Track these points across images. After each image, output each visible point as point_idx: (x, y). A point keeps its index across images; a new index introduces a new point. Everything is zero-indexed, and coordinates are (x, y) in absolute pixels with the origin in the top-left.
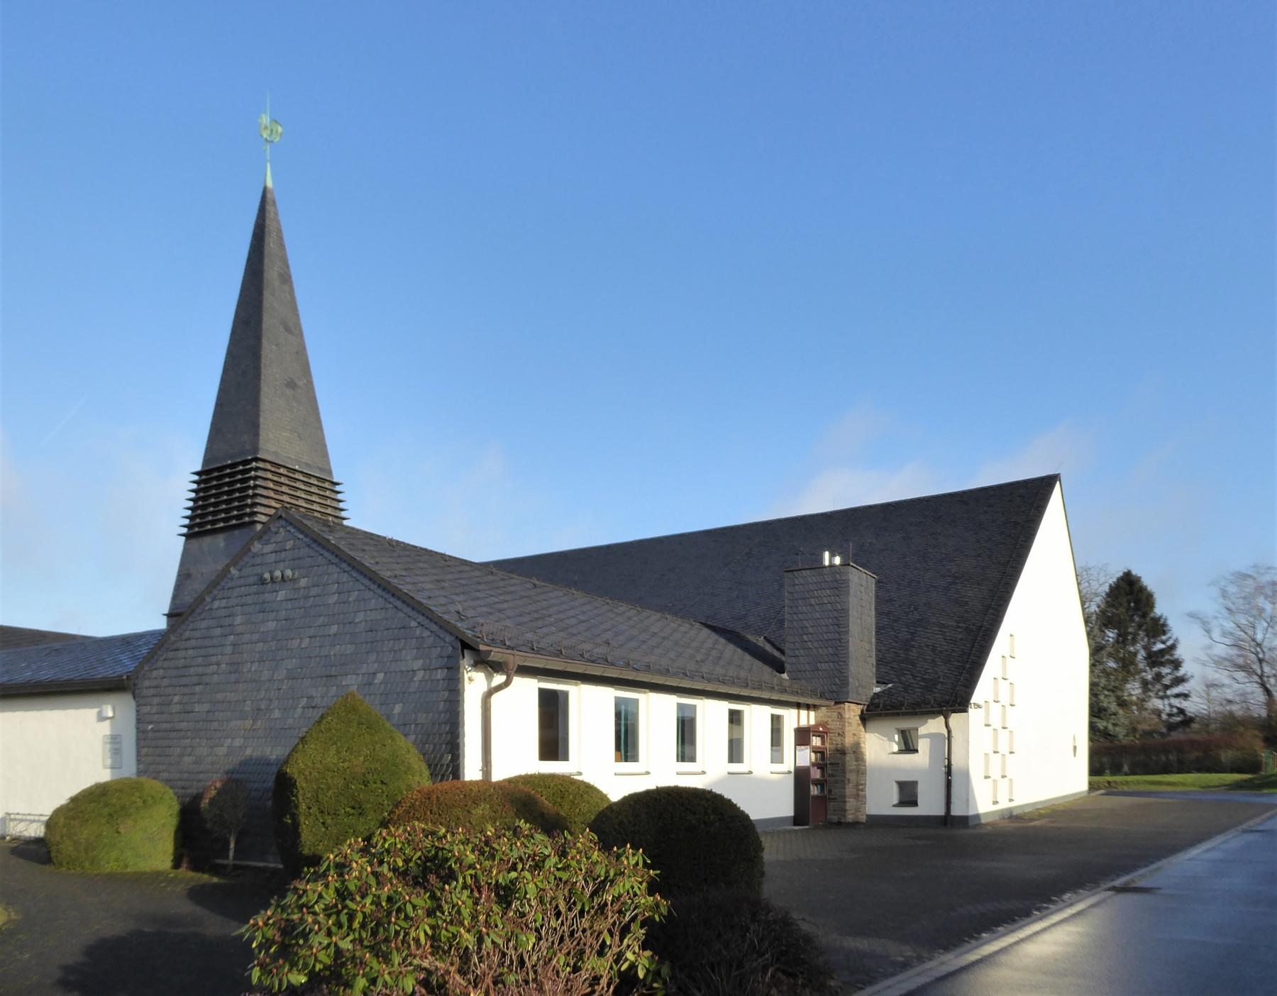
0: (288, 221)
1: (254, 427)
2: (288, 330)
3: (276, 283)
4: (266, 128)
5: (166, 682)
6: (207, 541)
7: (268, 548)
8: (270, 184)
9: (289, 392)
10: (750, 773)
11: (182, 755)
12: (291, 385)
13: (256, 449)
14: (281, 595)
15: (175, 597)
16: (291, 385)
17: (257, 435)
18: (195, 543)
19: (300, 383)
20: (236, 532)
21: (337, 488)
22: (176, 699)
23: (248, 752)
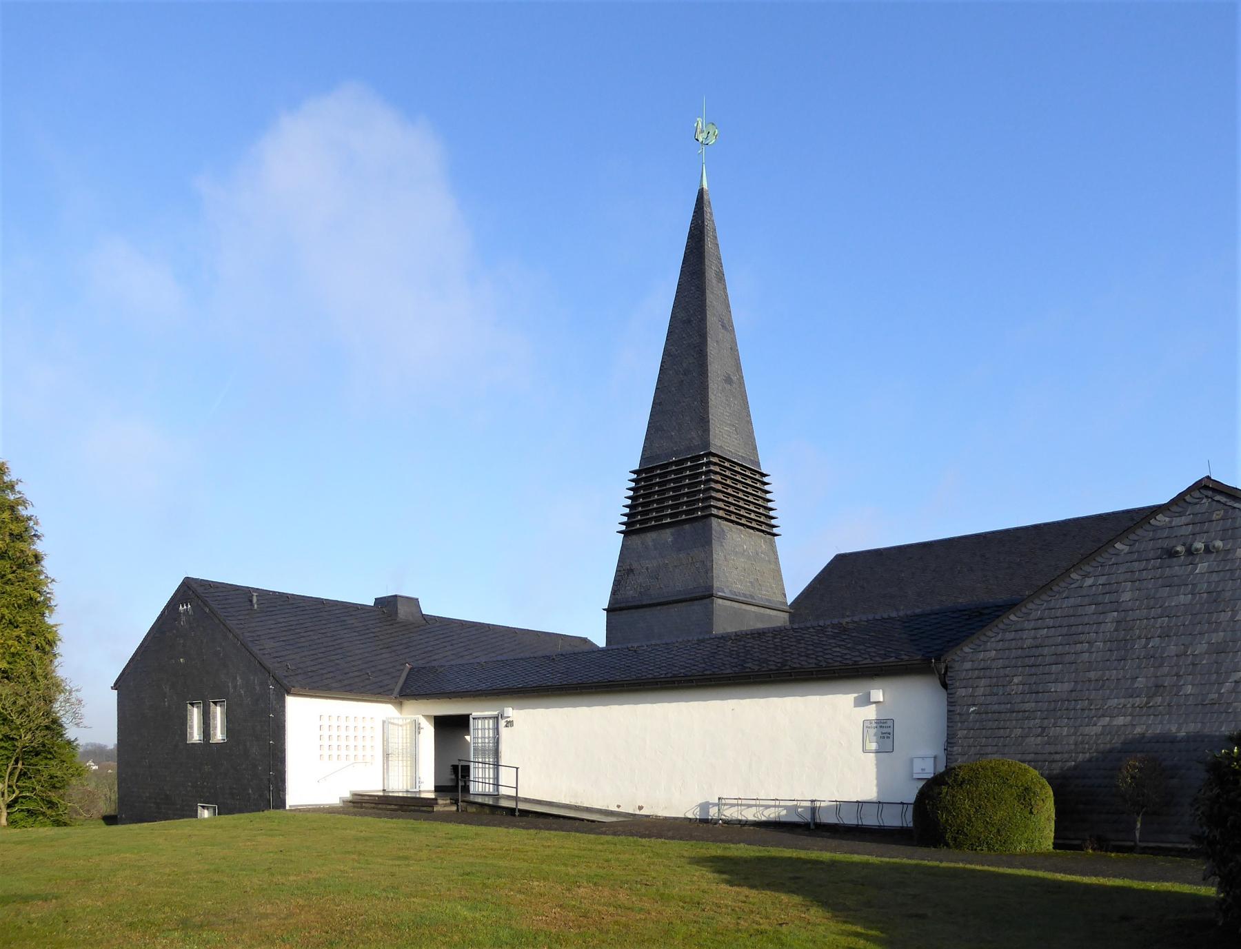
0: (718, 216)
1: (703, 422)
2: (723, 326)
3: (714, 281)
4: (702, 131)
5: (1000, 663)
6: (650, 537)
7: (1184, 520)
8: (705, 186)
9: (728, 387)
10: (935, 757)
11: (1023, 737)
12: (728, 380)
13: (707, 444)
14: (1202, 567)
15: (614, 592)
16: (728, 380)
17: (706, 430)
18: (636, 540)
19: (735, 378)
20: (687, 527)
21: (765, 479)
22: (1016, 680)
23: (1138, 730)
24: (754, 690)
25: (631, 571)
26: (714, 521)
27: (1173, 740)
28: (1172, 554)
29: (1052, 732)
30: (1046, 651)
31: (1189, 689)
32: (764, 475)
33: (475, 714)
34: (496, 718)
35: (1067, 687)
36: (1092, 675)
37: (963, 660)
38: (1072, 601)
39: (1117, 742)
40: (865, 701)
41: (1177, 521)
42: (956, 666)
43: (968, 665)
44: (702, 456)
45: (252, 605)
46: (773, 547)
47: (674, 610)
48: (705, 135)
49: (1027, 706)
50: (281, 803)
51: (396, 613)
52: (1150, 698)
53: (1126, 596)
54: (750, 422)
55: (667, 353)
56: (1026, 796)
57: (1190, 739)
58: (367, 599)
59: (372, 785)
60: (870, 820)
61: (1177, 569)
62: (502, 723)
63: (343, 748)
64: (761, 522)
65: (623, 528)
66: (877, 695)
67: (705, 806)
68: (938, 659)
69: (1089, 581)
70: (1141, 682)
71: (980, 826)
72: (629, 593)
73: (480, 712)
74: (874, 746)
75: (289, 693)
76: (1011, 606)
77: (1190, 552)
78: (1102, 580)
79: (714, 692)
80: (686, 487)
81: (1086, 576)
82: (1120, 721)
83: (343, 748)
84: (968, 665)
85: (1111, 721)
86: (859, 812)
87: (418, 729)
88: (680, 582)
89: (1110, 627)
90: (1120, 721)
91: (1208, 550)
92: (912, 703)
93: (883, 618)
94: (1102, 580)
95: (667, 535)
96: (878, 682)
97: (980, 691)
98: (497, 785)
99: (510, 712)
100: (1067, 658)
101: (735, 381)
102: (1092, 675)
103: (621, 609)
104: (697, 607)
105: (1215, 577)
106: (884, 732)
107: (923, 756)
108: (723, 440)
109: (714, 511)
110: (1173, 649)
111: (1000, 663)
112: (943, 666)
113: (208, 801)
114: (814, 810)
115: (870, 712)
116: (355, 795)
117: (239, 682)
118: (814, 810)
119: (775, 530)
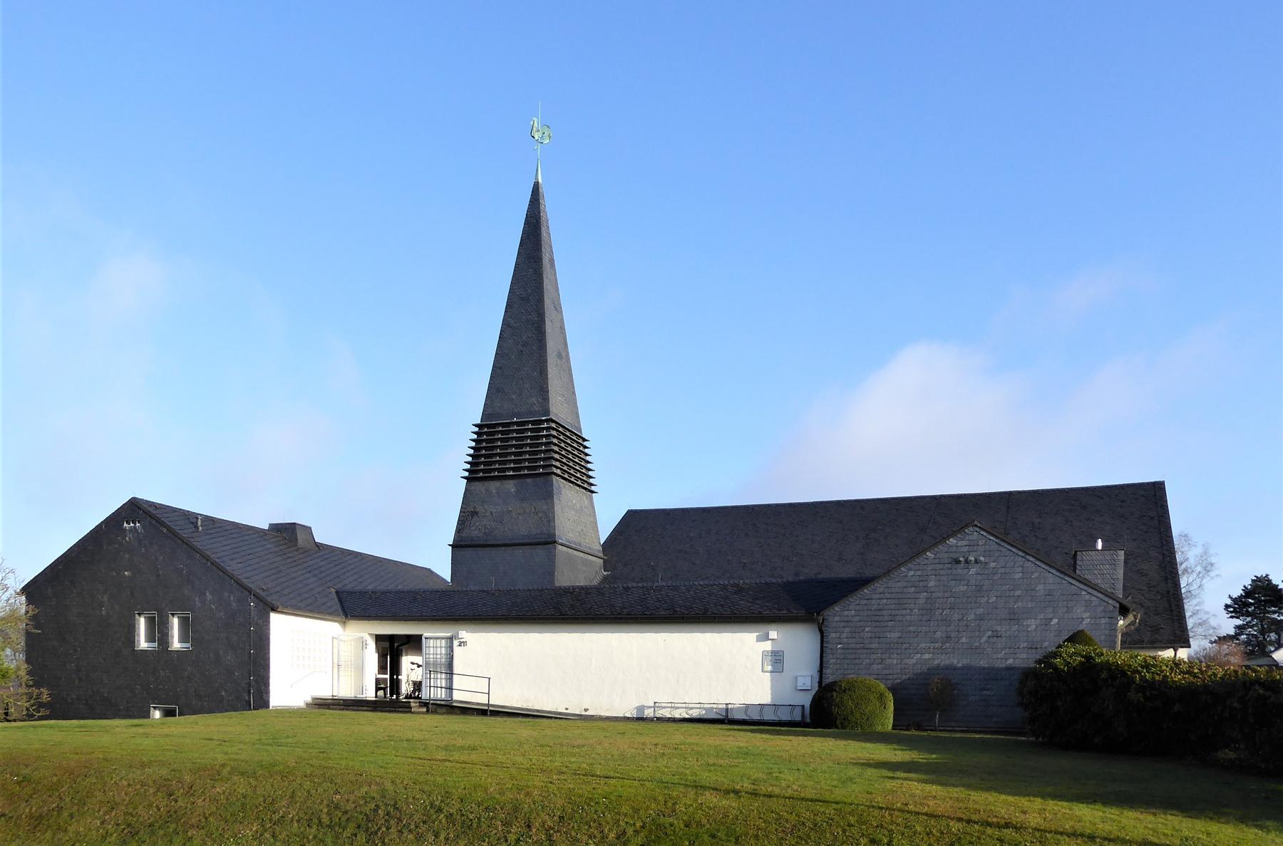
1: (543, 391)
5: (857, 618)
6: (494, 486)
13: (547, 412)
14: (973, 571)
15: (458, 531)
17: (546, 399)
18: (479, 486)
20: (529, 480)
24: (681, 627)
25: (474, 513)
26: (555, 478)
27: (955, 669)
28: (958, 562)
29: (888, 661)
30: (885, 613)
31: (964, 640)
32: (584, 440)
33: (426, 635)
34: (451, 639)
35: (897, 635)
36: (911, 629)
37: (835, 615)
38: (900, 584)
39: (925, 668)
40: (766, 638)
41: (960, 543)
42: (830, 619)
43: (837, 618)
44: (542, 422)
45: (196, 527)
46: (591, 499)
47: (519, 552)
48: (540, 134)
49: (873, 646)
50: (265, 704)
51: (296, 539)
52: (944, 643)
53: (932, 584)
54: (574, 393)
55: (505, 323)
56: (881, 697)
57: (963, 668)
58: (262, 522)
59: (326, 692)
60: (769, 716)
61: (960, 570)
62: (456, 643)
63: (314, 659)
64: (584, 483)
65: (467, 474)
66: (773, 634)
67: (641, 709)
68: (818, 614)
69: (912, 573)
70: (938, 634)
71: (858, 715)
72: (474, 533)
73: (434, 636)
74: (769, 668)
75: (274, 610)
76: (863, 582)
77: (967, 562)
78: (919, 573)
79: (728, 627)
80: (521, 446)
81: (910, 569)
82: (927, 656)
83: (314, 659)
84: (837, 618)
85: (922, 656)
86: (761, 711)
87: (364, 645)
88: (524, 527)
89: (923, 601)
90: (927, 656)
91: (976, 562)
92: (796, 641)
93: (680, 569)
94: (919, 573)
95: (511, 486)
96: (773, 626)
97: (844, 635)
98: (450, 688)
99: (464, 634)
100: (900, 618)
101: (564, 356)
102: (911, 629)
103: (462, 546)
104: (540, 551)
105: (979, 577)
106: (777, 659)
107: (803, 673)
108: (558, 410)
109: (555, 470)
110: (956, 617)
111: (857, 618)
112: (821, 618)
113: (158, 700)
114: (727, 710)
115: (767, 646)
116: (314, 699)
117: (209, 596)
118: (727, 710)
119: (593, 488)
